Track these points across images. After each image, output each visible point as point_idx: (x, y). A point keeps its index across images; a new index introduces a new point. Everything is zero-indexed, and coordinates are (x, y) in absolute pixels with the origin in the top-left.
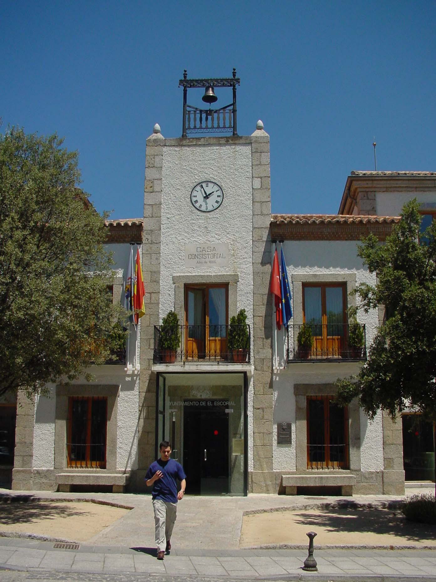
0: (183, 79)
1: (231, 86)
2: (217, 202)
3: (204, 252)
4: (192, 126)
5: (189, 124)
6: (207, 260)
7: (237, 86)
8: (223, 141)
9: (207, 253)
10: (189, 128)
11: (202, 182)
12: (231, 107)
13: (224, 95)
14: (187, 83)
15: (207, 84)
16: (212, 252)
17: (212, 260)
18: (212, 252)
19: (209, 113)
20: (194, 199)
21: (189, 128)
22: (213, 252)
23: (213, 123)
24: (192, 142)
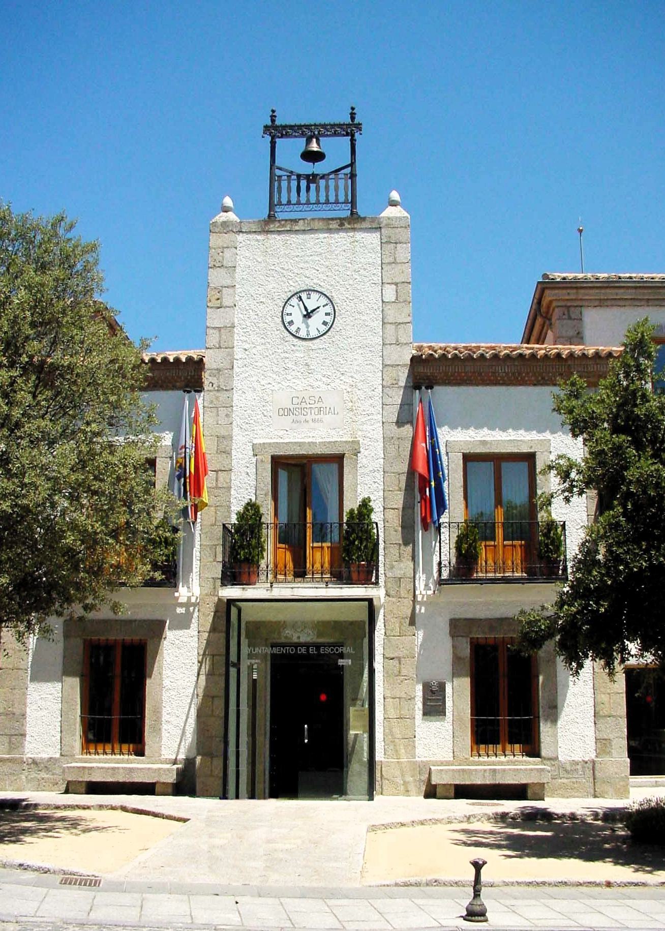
0: (270, 123)
1: (347, 134)
2: (325, 323)
3: (304, 405)
4: (284, 200)
5: (280, 198)
6: (308, 418)
7: (357, 135)
8: (334, 225)
9: (309, 406)
10: (280, 204)
11: (300, 292)
12: (348, 170)
13: (336, 151)
14: (276, 131)
15: (309, 132)
16: (316, 405)
17: (317, 417)
18: (316, 405)
19: (312, 179)
20: (287, 319)
21: (280, 204)
22: (319, 405)
23: (318, 195)
24: (283, 226)
